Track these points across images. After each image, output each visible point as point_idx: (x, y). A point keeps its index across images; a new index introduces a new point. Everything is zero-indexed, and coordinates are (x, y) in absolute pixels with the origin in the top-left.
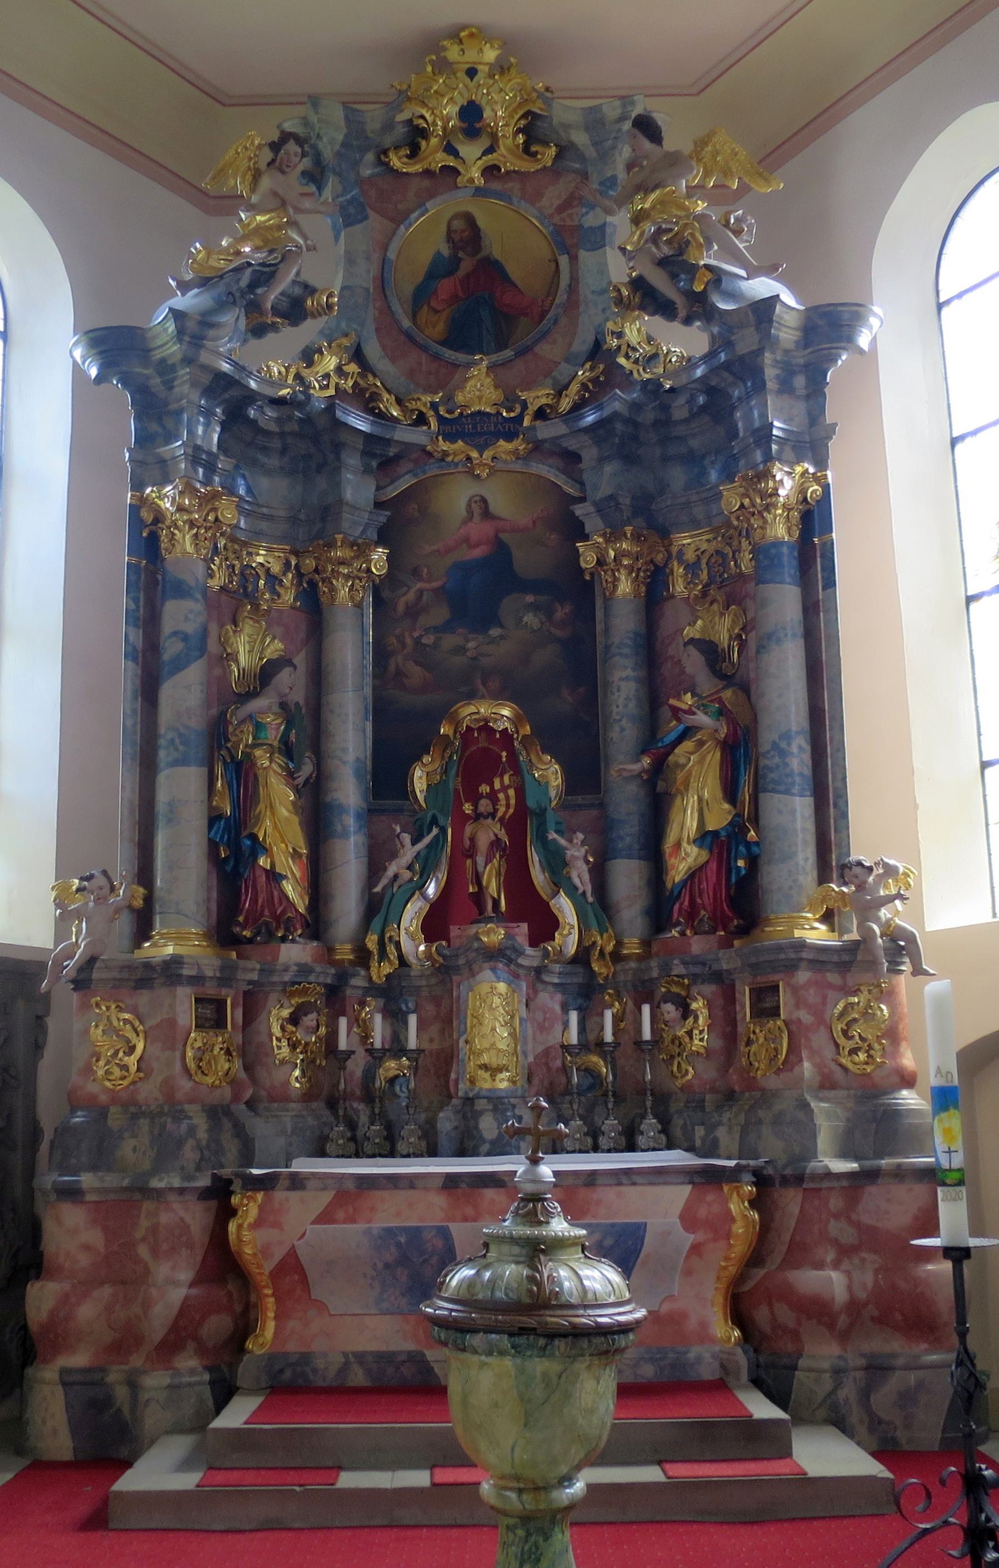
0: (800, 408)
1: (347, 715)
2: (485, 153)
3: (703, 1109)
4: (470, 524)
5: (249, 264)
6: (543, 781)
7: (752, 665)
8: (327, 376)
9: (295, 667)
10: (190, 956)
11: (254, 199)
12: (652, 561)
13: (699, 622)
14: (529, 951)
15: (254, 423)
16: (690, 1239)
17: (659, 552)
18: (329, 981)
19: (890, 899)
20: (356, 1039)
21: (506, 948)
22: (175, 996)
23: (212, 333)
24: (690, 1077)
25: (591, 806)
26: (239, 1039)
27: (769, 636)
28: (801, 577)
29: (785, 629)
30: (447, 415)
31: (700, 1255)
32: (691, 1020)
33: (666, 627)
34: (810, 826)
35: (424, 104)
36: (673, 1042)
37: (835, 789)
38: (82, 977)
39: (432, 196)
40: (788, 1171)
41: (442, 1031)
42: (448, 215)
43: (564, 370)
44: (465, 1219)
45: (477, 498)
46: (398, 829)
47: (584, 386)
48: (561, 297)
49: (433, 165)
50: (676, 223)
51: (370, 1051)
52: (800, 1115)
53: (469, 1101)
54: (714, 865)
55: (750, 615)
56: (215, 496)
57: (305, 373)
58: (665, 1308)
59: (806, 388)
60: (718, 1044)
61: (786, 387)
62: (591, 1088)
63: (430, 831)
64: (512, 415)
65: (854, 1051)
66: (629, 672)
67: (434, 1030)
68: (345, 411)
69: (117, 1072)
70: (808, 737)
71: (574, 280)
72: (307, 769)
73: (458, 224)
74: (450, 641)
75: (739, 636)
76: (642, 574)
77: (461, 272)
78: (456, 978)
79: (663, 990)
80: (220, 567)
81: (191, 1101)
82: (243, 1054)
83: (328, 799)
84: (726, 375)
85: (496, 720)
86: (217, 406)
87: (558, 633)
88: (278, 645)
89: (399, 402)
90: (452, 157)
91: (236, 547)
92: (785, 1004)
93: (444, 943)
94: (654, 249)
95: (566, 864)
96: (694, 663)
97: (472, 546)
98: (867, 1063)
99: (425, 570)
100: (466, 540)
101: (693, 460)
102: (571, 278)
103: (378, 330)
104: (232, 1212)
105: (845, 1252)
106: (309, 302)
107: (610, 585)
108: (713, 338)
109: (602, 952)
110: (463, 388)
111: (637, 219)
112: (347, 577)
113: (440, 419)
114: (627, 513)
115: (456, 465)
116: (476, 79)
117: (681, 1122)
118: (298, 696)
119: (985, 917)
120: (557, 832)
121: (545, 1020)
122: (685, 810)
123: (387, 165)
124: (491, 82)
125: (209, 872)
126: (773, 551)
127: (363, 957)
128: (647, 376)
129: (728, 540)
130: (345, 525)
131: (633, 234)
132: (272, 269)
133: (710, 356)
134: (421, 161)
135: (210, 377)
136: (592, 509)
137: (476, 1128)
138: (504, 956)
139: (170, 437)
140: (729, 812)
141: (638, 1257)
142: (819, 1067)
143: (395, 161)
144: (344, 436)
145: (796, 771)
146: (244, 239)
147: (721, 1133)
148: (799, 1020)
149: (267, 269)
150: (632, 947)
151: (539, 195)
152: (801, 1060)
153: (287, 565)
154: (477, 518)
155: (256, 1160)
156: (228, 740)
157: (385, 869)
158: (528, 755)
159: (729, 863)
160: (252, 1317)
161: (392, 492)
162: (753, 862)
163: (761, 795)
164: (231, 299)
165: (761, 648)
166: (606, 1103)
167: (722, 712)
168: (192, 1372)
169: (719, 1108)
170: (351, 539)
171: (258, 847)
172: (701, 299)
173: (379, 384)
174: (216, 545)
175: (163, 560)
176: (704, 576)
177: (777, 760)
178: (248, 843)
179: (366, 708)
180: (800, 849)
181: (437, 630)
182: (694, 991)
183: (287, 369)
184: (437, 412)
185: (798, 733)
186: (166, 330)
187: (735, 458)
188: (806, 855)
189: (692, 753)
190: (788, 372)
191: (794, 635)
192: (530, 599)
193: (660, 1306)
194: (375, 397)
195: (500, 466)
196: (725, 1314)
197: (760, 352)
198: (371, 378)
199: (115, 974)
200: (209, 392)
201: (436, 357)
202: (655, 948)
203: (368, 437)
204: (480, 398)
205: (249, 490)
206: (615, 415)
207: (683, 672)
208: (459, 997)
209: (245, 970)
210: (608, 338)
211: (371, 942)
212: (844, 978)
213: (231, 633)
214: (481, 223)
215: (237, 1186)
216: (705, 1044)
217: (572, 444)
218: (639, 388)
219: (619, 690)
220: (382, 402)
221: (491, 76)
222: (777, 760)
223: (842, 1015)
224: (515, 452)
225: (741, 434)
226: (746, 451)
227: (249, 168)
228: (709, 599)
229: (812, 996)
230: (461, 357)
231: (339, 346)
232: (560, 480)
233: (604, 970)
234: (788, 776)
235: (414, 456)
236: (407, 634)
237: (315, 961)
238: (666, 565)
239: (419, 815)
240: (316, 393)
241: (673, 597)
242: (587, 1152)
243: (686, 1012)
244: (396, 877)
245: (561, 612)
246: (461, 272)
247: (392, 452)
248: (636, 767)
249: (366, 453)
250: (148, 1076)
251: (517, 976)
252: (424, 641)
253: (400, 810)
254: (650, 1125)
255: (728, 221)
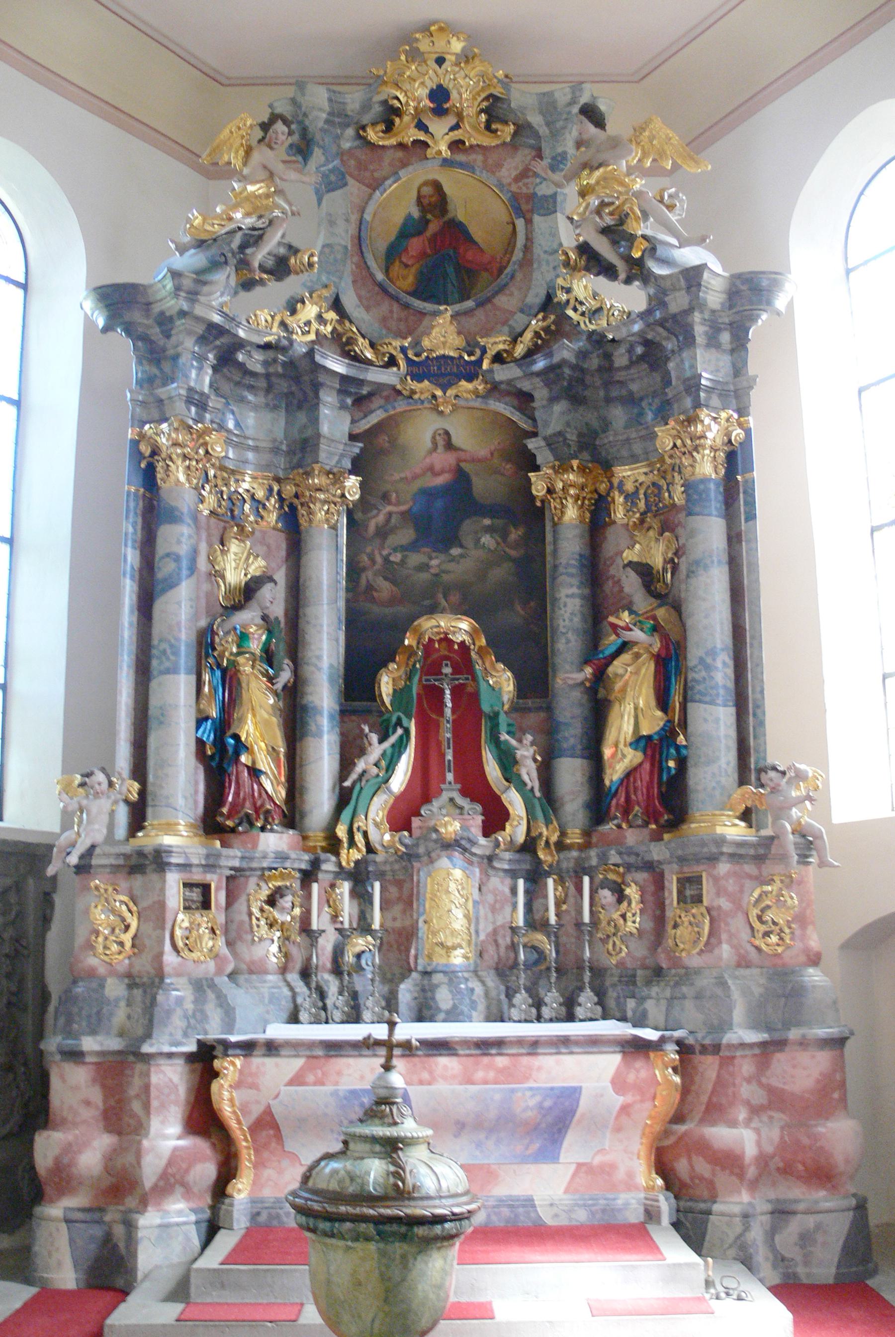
0: (725, 361)
1: (322, 626)
2: (452, 129)
3: (634, 983)
4: (434, 455)
5: (240, 229)
6: (497, 687)
7: (683, 586)
8: (308, 323)
9: (276, 583)
10: (178, 846)
11: (246, 171)
12: (596, 491)
13: (637, 546)
14: (482, 841)
15: (241, 366)
16: (619, 1100)
17: (602, 482)
18: (303, 866)
19: (800, 801)
20: (326, 918)
21: (462, 838)
22: (164, 881)
23: (206, 289)
24: (623, 954)
25: (540, 709)
26: (221, 919)
27: (697, 563)
28: (727, 509)
29: (711, 557)
30: (415, 358)
31: (628, 1115)
32: (625, 904)
33: (609, 547)
34: (733, 733)
35: (397, 86)
36: (609, 923)
37: (754, 701)
38: (83, 863)
39: (404, 164)
40: (707, 1041)
41: (404, 912)
42: (417, 183)
43: (519, 320)
44: (421, 1083)
45: (441, 432)
46: (366, 729)
47: (537, 335)
48: (518, 255)
49: (406, 139)
50: (618, 198)
51: (340, 931)
52: (719, 991)
53: (426, 974)
54: (647, 766)
55: (681, 542)
56: (206, 432)
57: (290, 321)
58: (598, 1160)
59: (731, 343)
60: (649, 925)
61: (713, 342)
62: (537, 962)
63: (394, 732)
64: (473, 358)
65: (767, 934)
66: (575, 590)
67: (397, 909)
68: (324, 356)
69: (115, 947)
70: (731, 654)
71: (529, 239)
72: (286, 676)
73: (427, 190)
74: (415, 559)
75: (672, 560)
76: (587, 502)
77: (429, 233)
78: (416, 865)
79: (601, 876)
80: (211, 492)
81: (179, 975)
82: (226, 932)
83: (304, 702)
84: (661, 330)
85: (454, 633)
86: (209, 352)
87: (513, 553)
88: (261, 562)
89: (372, 345)
90: (422, 133)
91: (225, 475)
92: (708, 892)
93: (406, 833)
94: (598, 219)
95: (516, 762)
96: (631, 583)
97: (436, 474)
98: (778, 945)
99: (394, 495)
100: (431, 469)
101: (631, 400)
102: (527, 239)
103: (354, 282)
104: (216, 1075)
105: (755, 1111)
106: (292, 261)
107: (559, 512)
108: (650, 298)
109: (547, 843)
110: (429, 334)
111: (583, 194)
112: (325, 502)
113: (409, 361)
114: (574, 448)
115: (422, 402)
116: (444, 66)
117: (615, 995)
118: (278, 610)
119: (885, 812)
120: (509, 733)
121: (496, 901)
122: (622, 716)
123: (364, 139)
124: (457, 69)
125: (196, 768)
126: (702, 487)
127: (333, 845)
128: (592, 327)
129: (663, 474)
130: (322, 456)
131: (580, 205)
132: (260, 232)
133: (649, 312)
134: (395, 135)
135: (203, 327)
136: (543, 443)
137: (433, 998)
138: (460, 846)
139: (167, 380)
140: (661, 719)
141: (574, 1116)
142: (736, 947)
143: (372, 135)
144: (322, 378)
145: (720, 684)
146: (235, 207)
147: (649, 1005)
148: (720, 907)
149: (256, 233)
150: (575, 837)
151: (499, 165)
152: (720, 942)
153: (271, 490)
154: (440, 449)
155: (237, 1026)
156: (214, 649)
157: (354, 764)
158: (484, 663)
159: (660, 762)
160: (233, 1165)
161: (365, 425)
162: (682, 763)
163: (689, 705)
164: (223, 259)
165: (690, 574)
166: (549, 977)
167: (656, 628)
168: (180, 1213)
169: (648, 983)
170: (328, 468)
171: (240, 746)
172: (639, 263)
173: (354, 329)
174: (207, 474)
175: (158, 488)
176: (642, 505)
177: (703, 674)
178: (232, 741)
179: (339, 619)
180: (723, 753)
181: (403, 548)
182: (628, 878)
183: (273, 317)
184: (406, 355)
185: (723, 650)
186: (164, 287)
187: (668, 403)
188: (727, 759)
189: (628, 665)
190: (715, 329)
191: (719, 562)
192: (487, 522)
193: (593, 1158)
194: (351, 341)
195: (462, 403)
196: (649, 1166)
197: (689, 311)
198: (347, 324)
199: (113, 861)
200: (202, 340)
201: (406, 306)
202: (594, 840)
203: (344, 378)
204: (444, 343)
205: (238, 425)
206: (563, 362)
207: (621, 589)
208: (418, 882)
209: (228, 857)
210: (559, 293)
211: (341, 831)
212: (759, 868)
213: (219, 552)
214: (447, 189)
215: (218, 1052)
216: (637, 925)
217: (526, 386)
218: (584, 338)
219: (565, 606)
220: (357, 345)
221: (457, 64)
222: (703, 674)
223: (758, 901)
224: (476, 392)
225: (674, 383)
226: (678, 398)
227: (242, 145)
228: (646, 525)
229: (731, 885)
230: (428, 306)
231: (320, 297)
232: (516, 417)
233: (549, 859)
234: (712, 688)
235: (385, 393)
236: (376, 552)
237: (292, 848)
238: (608, 494)
239: (385, 717)
240: (298, 338)
241: (614, 522)
242: (532, 1022)
243: (621, 897)
244: (364, 772)
245: (515, 534)
246: (429, 233)
247: (364, 391)
248: (579, 677)
249: (342, 392)
250: (141, 951)
251: (471, 863)
252: (392, 558)
253: (370, 712)
254: (587, 999)
255: (662, 197)
